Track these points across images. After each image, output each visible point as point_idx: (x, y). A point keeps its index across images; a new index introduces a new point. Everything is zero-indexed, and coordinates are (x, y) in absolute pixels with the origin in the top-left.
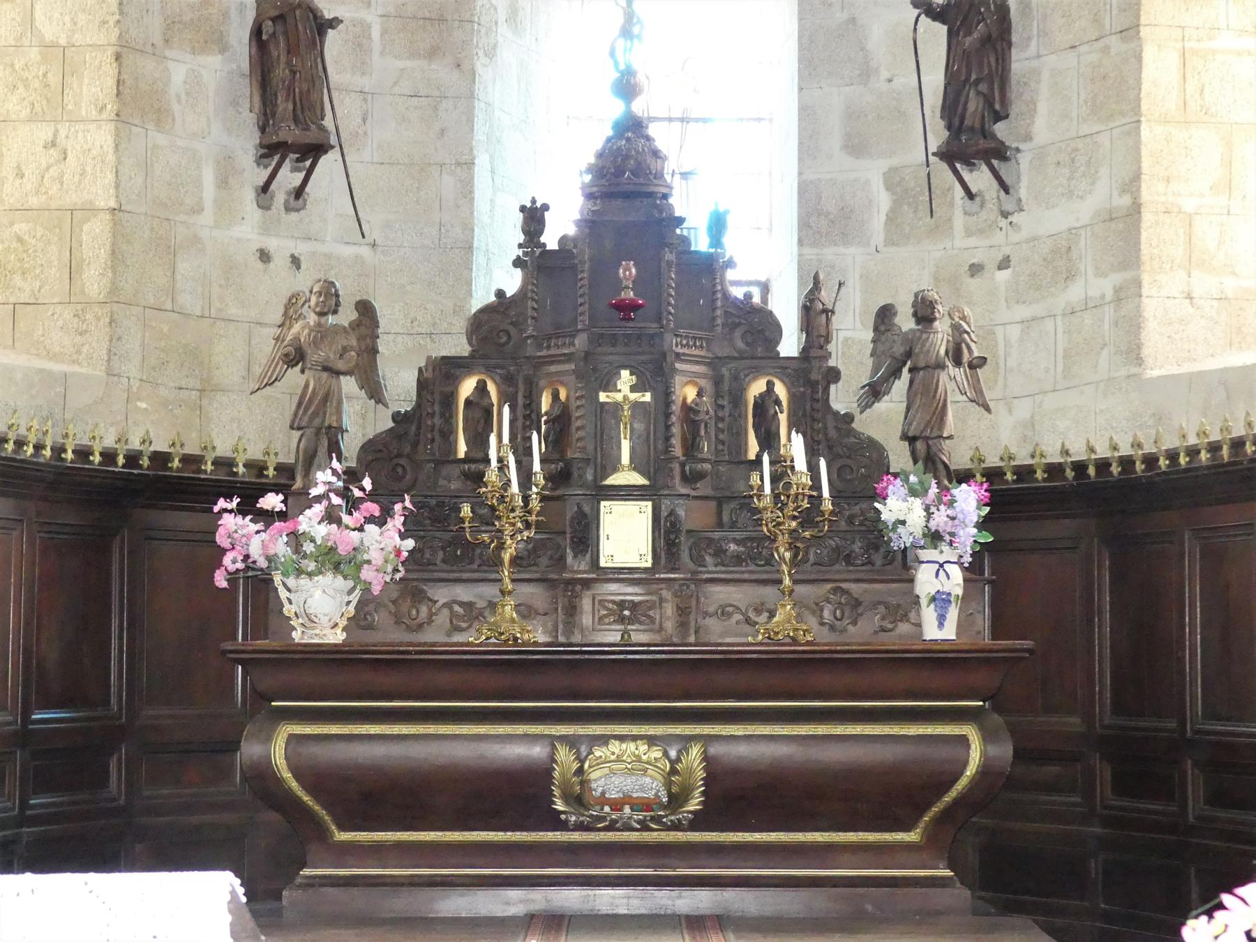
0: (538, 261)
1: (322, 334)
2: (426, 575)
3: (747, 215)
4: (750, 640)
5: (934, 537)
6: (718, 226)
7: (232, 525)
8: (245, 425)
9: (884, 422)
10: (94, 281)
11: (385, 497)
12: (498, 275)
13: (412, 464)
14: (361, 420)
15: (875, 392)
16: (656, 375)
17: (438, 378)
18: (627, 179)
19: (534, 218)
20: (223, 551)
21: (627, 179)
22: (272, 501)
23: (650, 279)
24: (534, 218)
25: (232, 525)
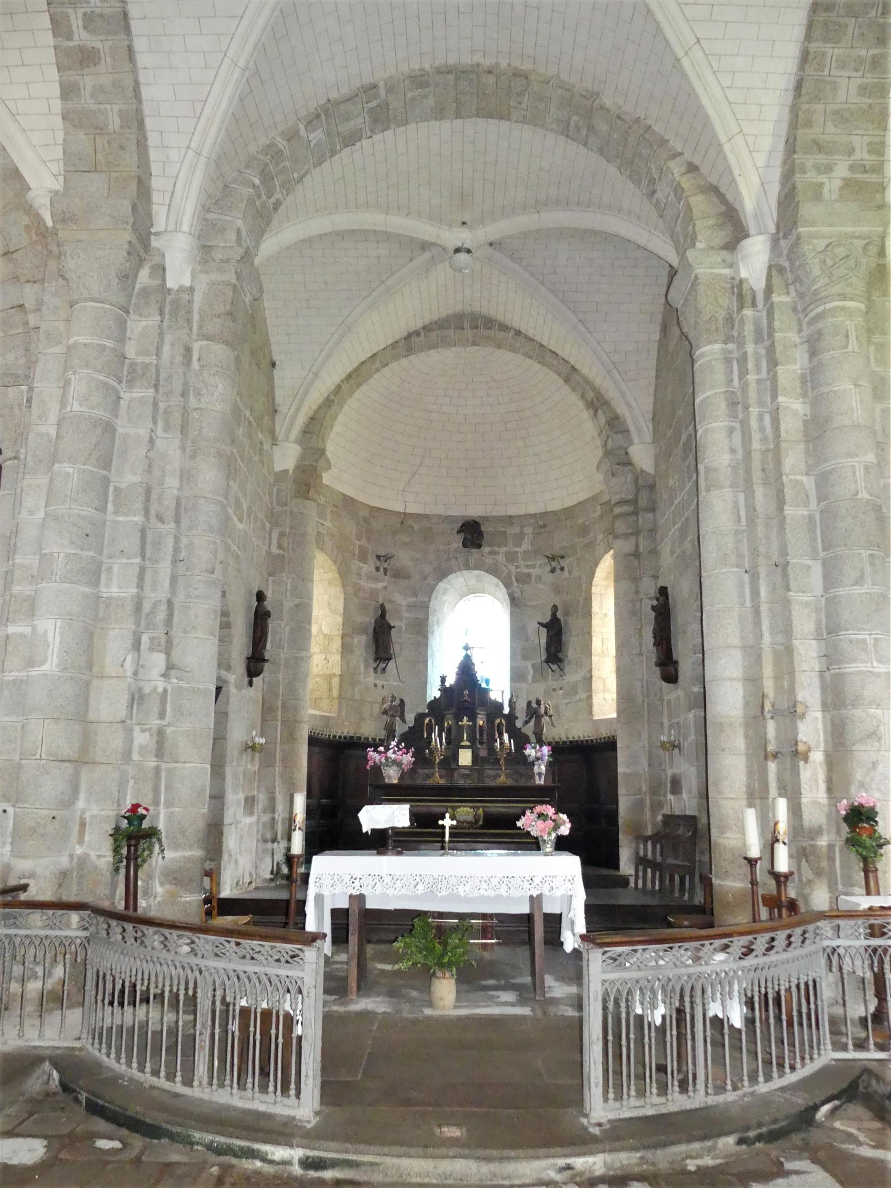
0: (444, 690)
1: (391, 707)
3: (498, 684)
7: (372, 754)
8: (370, 729)
9: (529, 730)
10: (335, 693)
11: (407, 748)
12: (434, 692)
13: (414, 738)
14: (400, 728)
15: (526, 722)
16: (473, 718)
17: (420, 718)
18: (466, 670)
19: (443, 679)
21: (466, 670)
22: (381, 749)
24: (443, 679)
25: (372, 754)
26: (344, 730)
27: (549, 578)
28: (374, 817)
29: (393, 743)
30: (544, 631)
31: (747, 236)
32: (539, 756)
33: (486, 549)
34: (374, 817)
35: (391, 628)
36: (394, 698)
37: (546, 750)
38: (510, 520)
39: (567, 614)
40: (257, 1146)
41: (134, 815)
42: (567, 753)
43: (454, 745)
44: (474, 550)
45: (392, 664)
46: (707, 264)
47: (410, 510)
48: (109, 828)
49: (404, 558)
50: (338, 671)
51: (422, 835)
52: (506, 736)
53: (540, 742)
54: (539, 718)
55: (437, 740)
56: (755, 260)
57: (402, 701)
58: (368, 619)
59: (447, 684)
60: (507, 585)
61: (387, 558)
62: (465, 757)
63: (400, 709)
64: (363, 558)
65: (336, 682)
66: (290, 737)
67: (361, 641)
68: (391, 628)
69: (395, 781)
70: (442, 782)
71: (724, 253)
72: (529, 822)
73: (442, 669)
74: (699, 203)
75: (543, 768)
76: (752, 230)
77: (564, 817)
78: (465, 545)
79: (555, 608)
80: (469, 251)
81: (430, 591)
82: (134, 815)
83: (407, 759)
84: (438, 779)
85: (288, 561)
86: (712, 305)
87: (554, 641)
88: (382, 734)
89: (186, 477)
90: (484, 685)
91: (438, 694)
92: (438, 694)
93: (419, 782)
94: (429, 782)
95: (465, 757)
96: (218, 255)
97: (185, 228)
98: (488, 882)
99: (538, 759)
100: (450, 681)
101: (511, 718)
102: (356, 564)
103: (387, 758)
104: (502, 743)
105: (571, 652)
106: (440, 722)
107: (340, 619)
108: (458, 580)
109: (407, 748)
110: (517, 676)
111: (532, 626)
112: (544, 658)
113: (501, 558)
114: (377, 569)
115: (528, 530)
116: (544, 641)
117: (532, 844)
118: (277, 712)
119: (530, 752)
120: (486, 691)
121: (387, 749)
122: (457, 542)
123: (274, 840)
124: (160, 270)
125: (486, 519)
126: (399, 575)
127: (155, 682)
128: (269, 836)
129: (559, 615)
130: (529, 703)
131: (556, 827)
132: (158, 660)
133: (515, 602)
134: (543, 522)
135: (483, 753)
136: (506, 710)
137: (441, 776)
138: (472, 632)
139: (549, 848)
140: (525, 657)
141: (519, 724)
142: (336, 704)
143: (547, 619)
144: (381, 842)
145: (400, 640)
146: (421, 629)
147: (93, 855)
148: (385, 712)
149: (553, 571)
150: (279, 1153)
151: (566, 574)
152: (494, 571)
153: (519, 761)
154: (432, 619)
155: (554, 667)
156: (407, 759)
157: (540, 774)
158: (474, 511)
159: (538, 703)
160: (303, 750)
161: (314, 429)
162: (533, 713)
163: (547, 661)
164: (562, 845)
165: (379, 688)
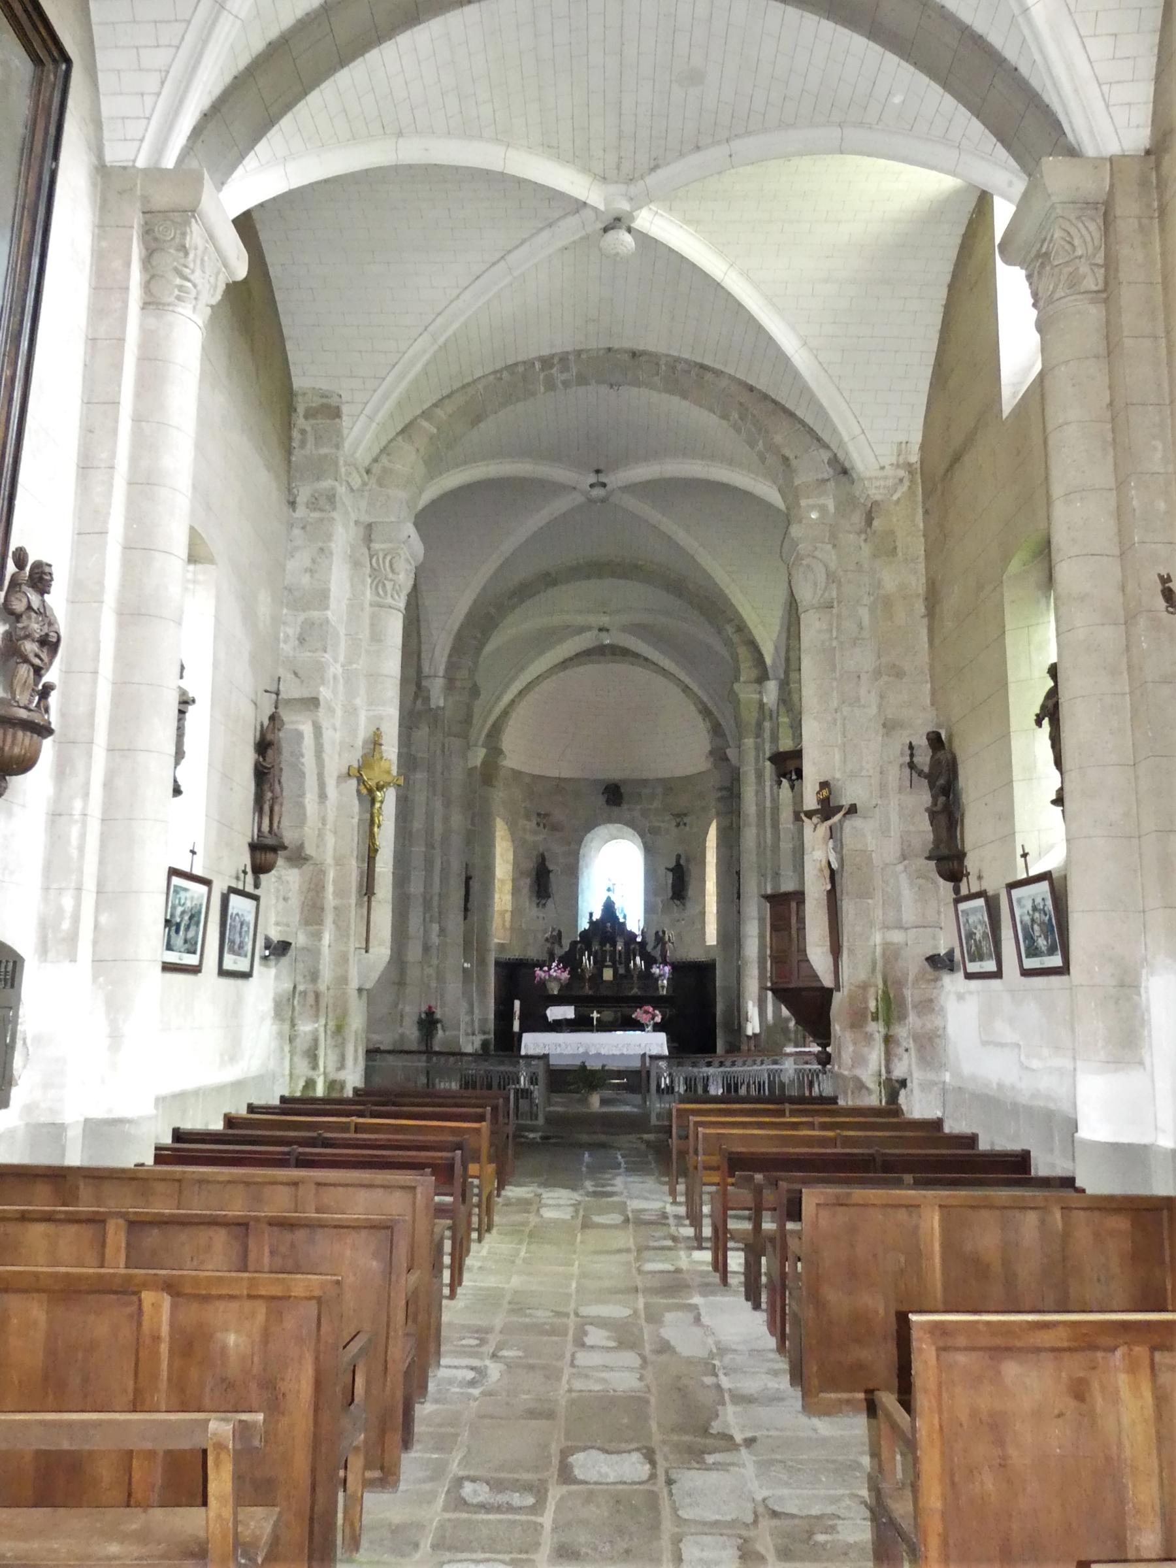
0: (591, 922)
1: (552, 936)
2: (796, 973)
3: (634, 920)
4: (446, 1091)
5: (853, 775)
6: (625, 917)
7: (538, 972)
8: (533, 953)
9: (657, 953)
10: (508, 924)
11: (565, 968)
12: (584, 924)
13: (570, 961)
14: (559, 952)
15: (655, 947)
16: (614, 945)
17: (574, 944)
18: (609, 907)
19: (591, 915)
20: (657, 980)
21: (609, 907)
22: (546, 968)
23: (613, 927)
24: (591, 915)
25: (538, 972)
26: (515, 954)
27: (674, 830)
28: (555, 1013)
29: (554, 964)
30: (670, 875)
31: (768, 679)
32: (662, 971)
33: (625, 807)
34: (555, 1013)
35: (549, 872)
36: (553, 929)
37: (667, 969)
38: (645, 782)
39: (688, 860)
40: (998, 240)
41: (430, 1013)
42: (681, 969)
43: (599, 965)
44: (615, 808)
45: (550, 900)
46: (746, 693)
47: (563, 775)
48: (416, 1019)
49: (558, 815)
50: (509, 907)
51: (580, 1024)
52: (638, 959)
53: (665, 963)
54: (664, 944)
55: (587, 961)
56: (771, 690)
57: (560, 933)
58: (530, 865)
59: (594, 919)
60: (642, 836)
61: (546, 815)
62: (608, 974)
63: (558, 938)
64: (528, 818)
65: (508, 916)
66: (482, 962)
67: (526, 882)
68: (549, 872)
69: (556, 993)
70: (590, 993)
71: (756, 685)
72: (639, 1015)
73: (590, 907)
74: (743, 652)
75: (665, 982)
76: (771, 676)
77: (657, 1012)
78: (608, 802)
79: (679, 857)
80: (608, 630)
81: (580, 842)
82: (430, 1013)
83: (565, 975)
84: (587, 991)
85: (478, 839)
86: (750, 716)
87: (674, 883)
88: (545, 957)
89: (446, 819)
90: (622, 920)
91: (587, 926)
92: (587, 926)
93: (574, 993)
94: (581, 993)
95: (608, 974)
96: (458, 684)
97: (441, 673)
98: (617, 1046)
99: (660, 976)
100: (597, 916)
101: (643, 944)
102: (522, 822)
103: (550, 976)
104: (635, 964)
105: (691, 892)
106: (588, 947)
107: (510, 868)
108: (602, 831)
109: (565, 968)
110: (649, 909)
111: (661, 871)
112: (670, 894)
113: (637, 814)
114: (538, 824)
115: (659, 790)
116: (670, 881)
117: (638, 1026)
118: (475, 942)
119: (655, 970)
120: (624, 924)
121: (550, 969)
122: (601, 800)
123: (473, 1034)
124: (427, 699)
125: (625, 781)
126: (555, 828)
127: (435, 940)
128: (470, 1031)
129: (682, 862)
130: (657, 933)
131: (653, 1019)
132: (435, 927)
133: (649, 850)
134: (670, 786)
135: (622, 971)
136: (639, 939)
137: (590, 988)
138: (614, 876)
139: (650, 1028)
140: (656, 894)
141: (649, 948)
142: (508, 933)
143: (672, 864)
144: (559, 1026)
145: (556, 882)
146: (573, 872)
147: (408, 1032)
148: (547, 940)
149: (678, 825)
150: (531, 1135)
151: (687, 828)
152: (631, 824)
153: (648, 978)
154: (581, 863)
155: (678, 902)
156: (565, 975)
157: (663, 987)
158: (614, 774)
159: (664, 932)
160: (492, 970)
161: (496, 731)
162: (660, 939)
163: (672, 898)
164: (657, 1028)
165: (541, 920)
